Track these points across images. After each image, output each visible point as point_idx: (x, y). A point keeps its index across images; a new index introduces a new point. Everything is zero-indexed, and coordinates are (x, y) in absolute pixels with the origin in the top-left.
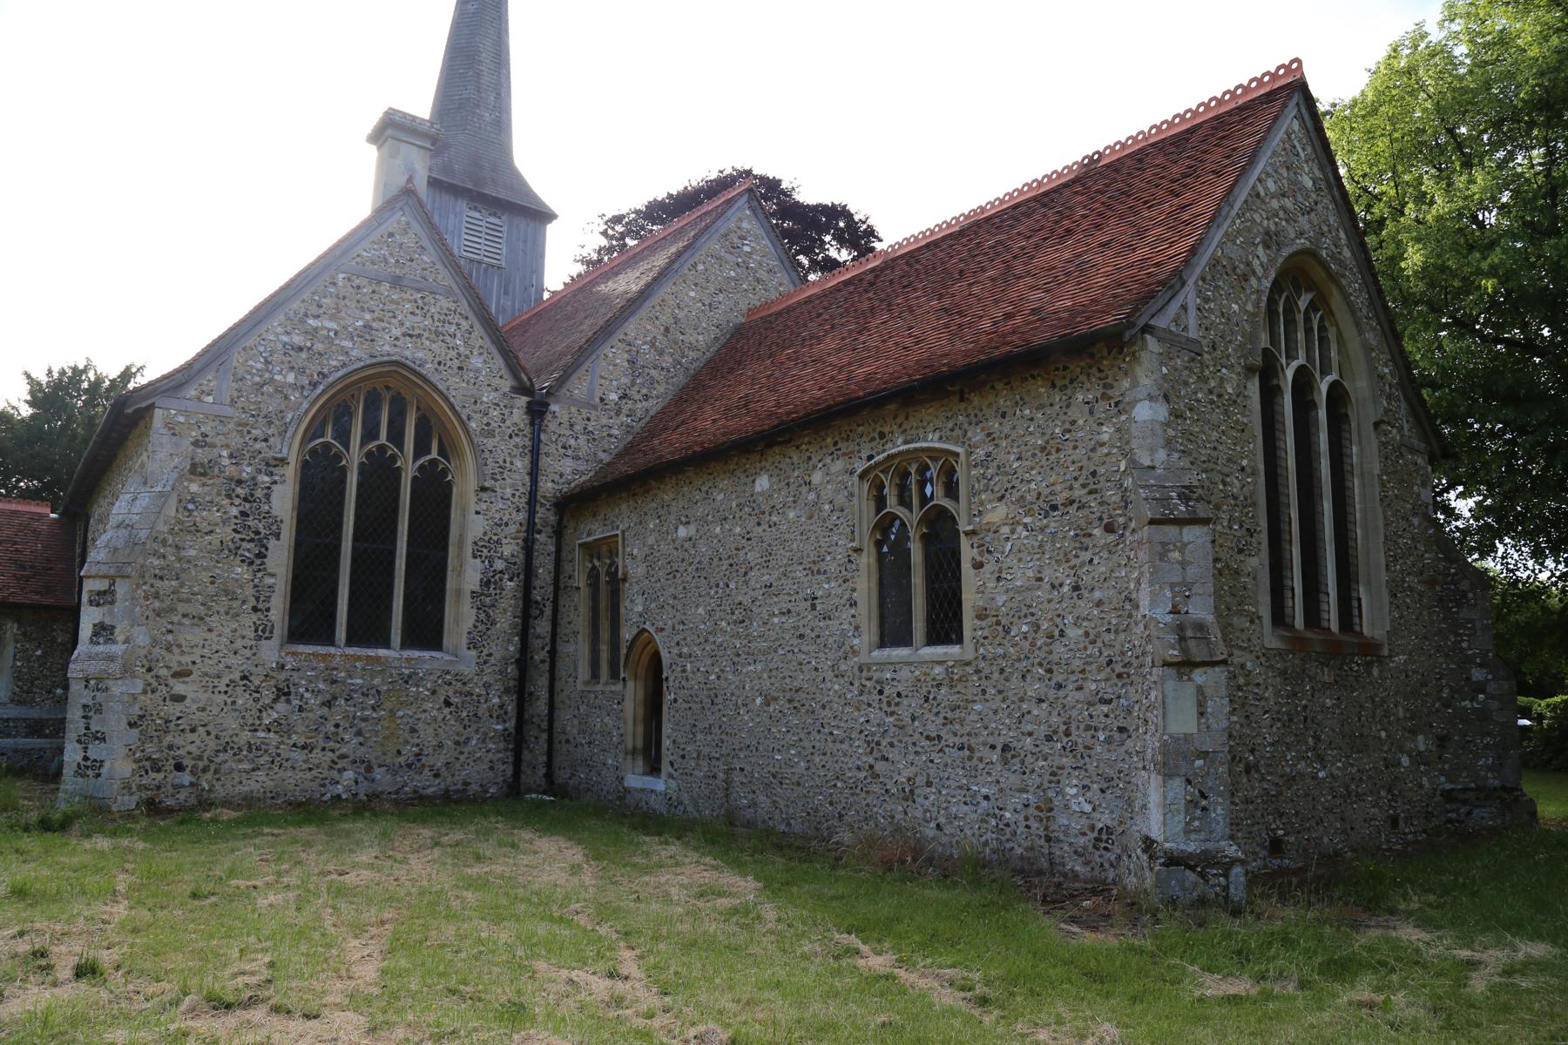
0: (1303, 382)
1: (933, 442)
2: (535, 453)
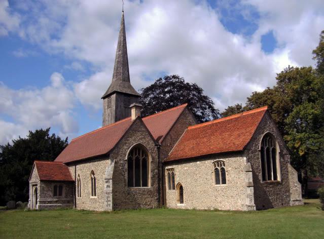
1: (221, 160)
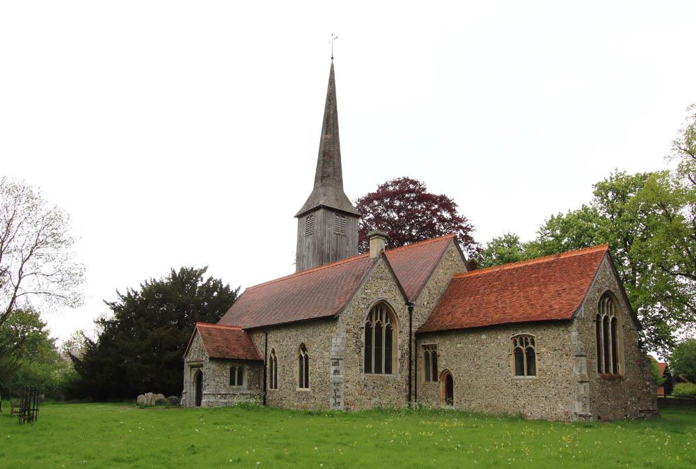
0: (606, 318)
2: (411, 320)
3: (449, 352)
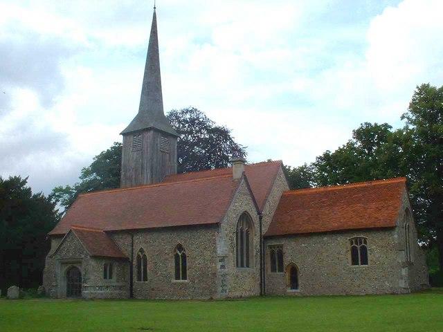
1: (362, 236)
3: (292, 251)
